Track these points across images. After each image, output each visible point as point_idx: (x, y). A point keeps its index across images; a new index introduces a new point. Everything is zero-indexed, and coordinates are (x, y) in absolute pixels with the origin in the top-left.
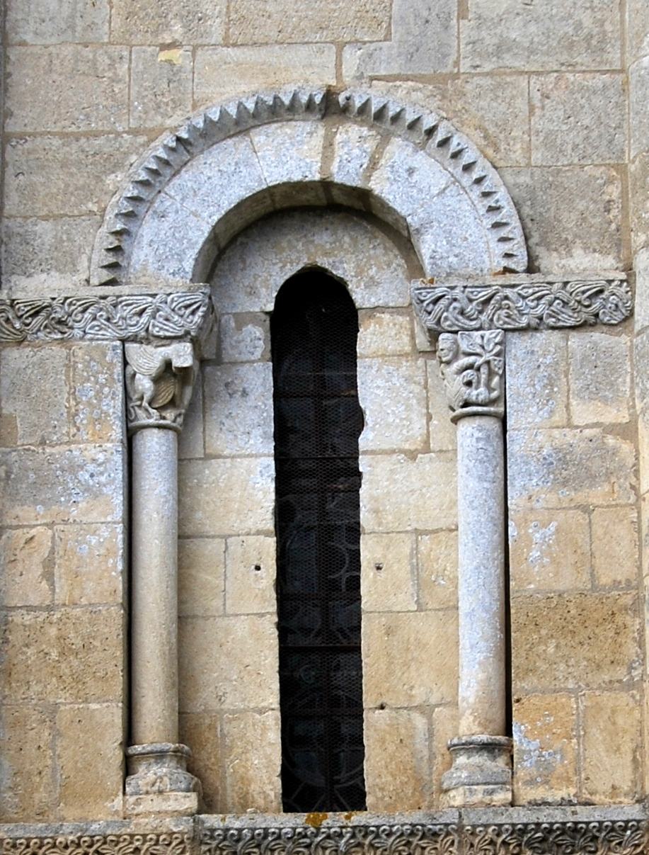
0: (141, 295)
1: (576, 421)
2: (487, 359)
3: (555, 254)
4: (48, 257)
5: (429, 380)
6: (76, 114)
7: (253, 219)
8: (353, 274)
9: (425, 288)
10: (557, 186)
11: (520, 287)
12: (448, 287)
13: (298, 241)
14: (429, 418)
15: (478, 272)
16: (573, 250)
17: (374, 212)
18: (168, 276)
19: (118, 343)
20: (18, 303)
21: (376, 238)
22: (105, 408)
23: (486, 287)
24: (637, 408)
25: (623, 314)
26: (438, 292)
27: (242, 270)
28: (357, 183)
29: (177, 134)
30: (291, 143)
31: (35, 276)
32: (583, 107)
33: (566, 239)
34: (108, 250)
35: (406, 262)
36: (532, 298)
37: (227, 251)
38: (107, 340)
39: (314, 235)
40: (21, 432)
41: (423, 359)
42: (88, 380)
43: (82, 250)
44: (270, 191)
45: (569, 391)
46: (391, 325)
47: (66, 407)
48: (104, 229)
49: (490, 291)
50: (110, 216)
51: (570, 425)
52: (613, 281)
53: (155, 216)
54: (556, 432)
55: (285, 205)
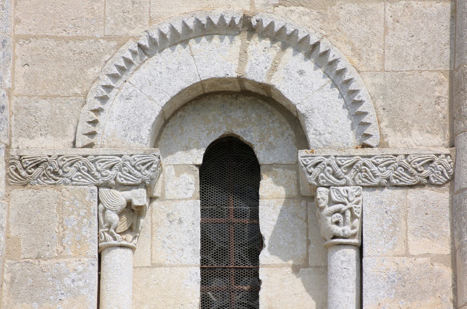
0: (111, 155)
1: (412, 252)
2: (350, 206)
3: (399, 134)
4: (45, 125)
5: (309, 216)
6: (66, 24)
7: (188, 100)
8: (258, 140)
9: (307, 157)
10: (402, 86)
11: (374, 158)
12: (324, 156)
13: (220, 115)
14: (309, 243)
15: (345, 145)
16: (412, 131)
17: (273, 97)
18: (131, 141)
19: (95, 188)
20: (24, 158)
21: (274, 115)
22: (84, 233)
24: (456, 245)
25: (446, 178)
26: (316, 160)
27: (180, 135)
28: (261, 78)
29: (138, 42)
30: (218, 50)
31: (36, 138)
32: (422, 29)
33: (407, 123)
34: (89, 122)
35: (295, 133)
36: (382, 165)
37: (170, 121)
38: (86, 185)
39: (231, 112)
40: (23, 249)
41: (305, 202)
42: (72, 213)
43: (70, 122)
44: (202, 83)
45: (407, 230)
46: (283, 176)
47: (56, 232)
48: (86, 107)
49: (354, 159)
50: (91, 98)
51: (407, 255)
52: (440, 155)
53: (122, 98)
54: (397, 259)
55: (211, 91)
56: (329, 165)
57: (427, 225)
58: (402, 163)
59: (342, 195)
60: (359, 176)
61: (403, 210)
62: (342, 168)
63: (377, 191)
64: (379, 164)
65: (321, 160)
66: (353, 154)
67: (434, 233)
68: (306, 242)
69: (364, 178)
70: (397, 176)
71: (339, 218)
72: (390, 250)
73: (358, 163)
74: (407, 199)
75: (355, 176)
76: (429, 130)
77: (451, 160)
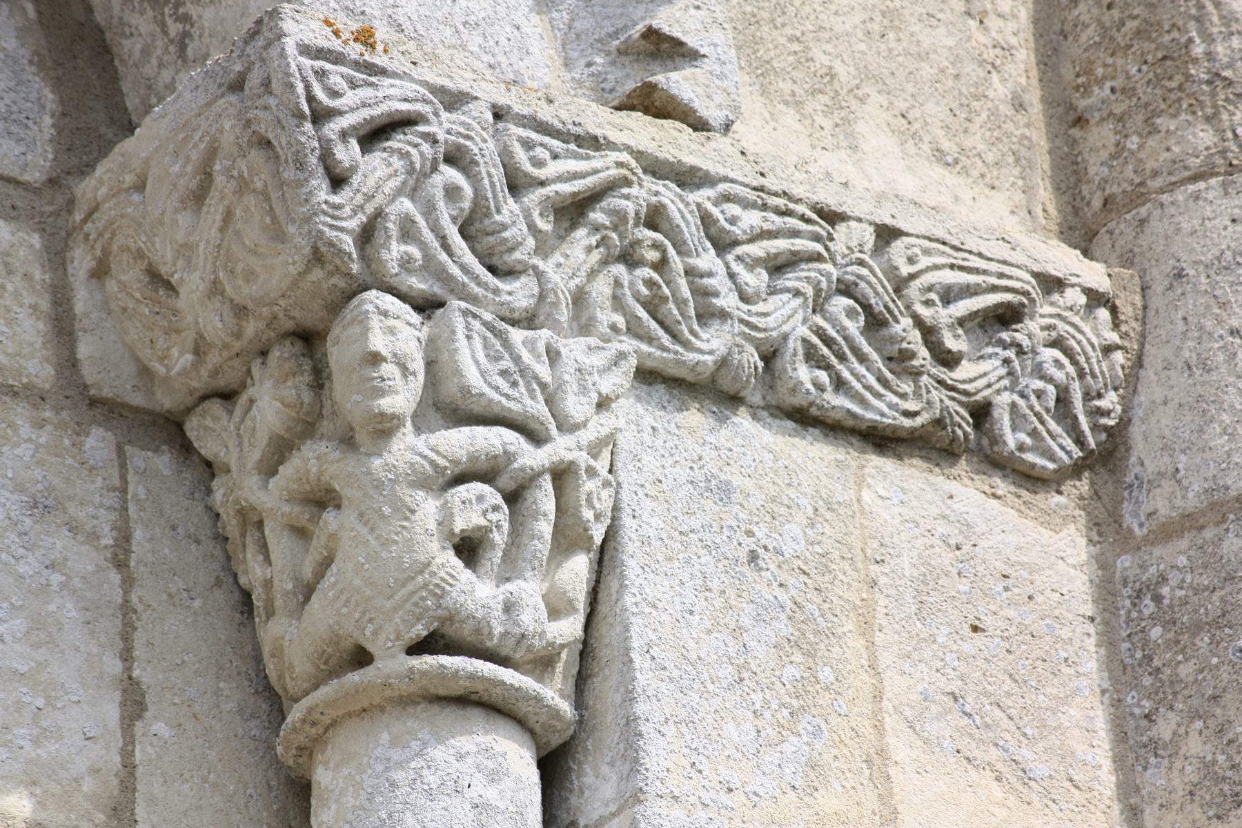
3: (789, 117)
5: (138, 534)
9: (337, 58)
23: (579, 140)
33: (831, 75)
36: (756, 250)
45: (878, 697)
49: (604, 165)
56: (455, 157)
57: (986, 694)
58: (864, 272)
59: (523, 371)
60: (617, 283)
61: (846, 565)
62: (534, 197)
63: (695, 418)
64: (736, 243)
65: (418, 107)
66: (598, 132)
67: (1024, 751)
68: (117, 696)
69: (646, 305)
70: (825, 351)
71: (491, 516)
72: (792, 795)
73: (627, 197)
74: (862, 511)
75: (592, 274)
76: (946, 145)
77: (1114, 337)
